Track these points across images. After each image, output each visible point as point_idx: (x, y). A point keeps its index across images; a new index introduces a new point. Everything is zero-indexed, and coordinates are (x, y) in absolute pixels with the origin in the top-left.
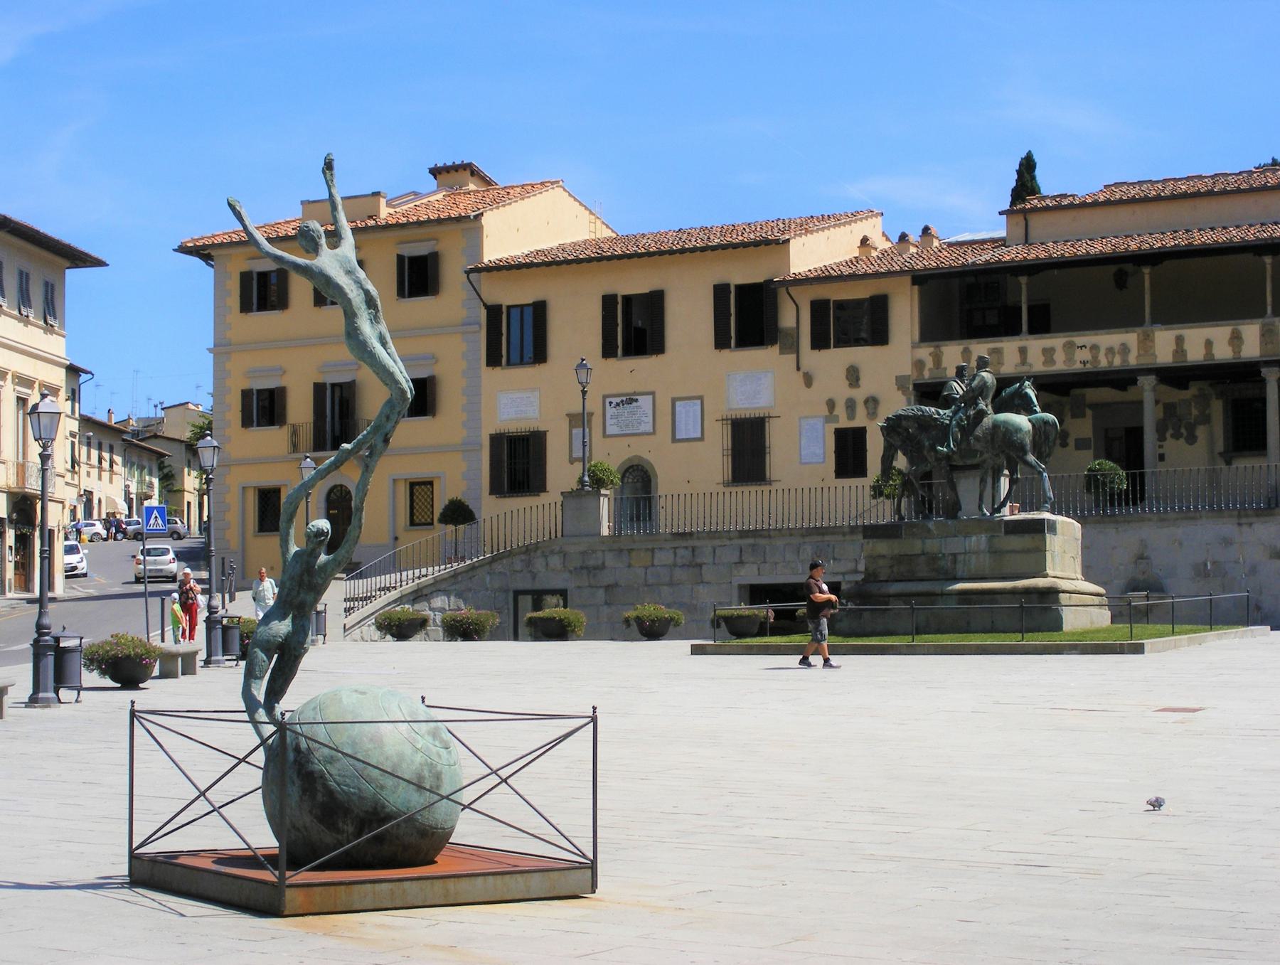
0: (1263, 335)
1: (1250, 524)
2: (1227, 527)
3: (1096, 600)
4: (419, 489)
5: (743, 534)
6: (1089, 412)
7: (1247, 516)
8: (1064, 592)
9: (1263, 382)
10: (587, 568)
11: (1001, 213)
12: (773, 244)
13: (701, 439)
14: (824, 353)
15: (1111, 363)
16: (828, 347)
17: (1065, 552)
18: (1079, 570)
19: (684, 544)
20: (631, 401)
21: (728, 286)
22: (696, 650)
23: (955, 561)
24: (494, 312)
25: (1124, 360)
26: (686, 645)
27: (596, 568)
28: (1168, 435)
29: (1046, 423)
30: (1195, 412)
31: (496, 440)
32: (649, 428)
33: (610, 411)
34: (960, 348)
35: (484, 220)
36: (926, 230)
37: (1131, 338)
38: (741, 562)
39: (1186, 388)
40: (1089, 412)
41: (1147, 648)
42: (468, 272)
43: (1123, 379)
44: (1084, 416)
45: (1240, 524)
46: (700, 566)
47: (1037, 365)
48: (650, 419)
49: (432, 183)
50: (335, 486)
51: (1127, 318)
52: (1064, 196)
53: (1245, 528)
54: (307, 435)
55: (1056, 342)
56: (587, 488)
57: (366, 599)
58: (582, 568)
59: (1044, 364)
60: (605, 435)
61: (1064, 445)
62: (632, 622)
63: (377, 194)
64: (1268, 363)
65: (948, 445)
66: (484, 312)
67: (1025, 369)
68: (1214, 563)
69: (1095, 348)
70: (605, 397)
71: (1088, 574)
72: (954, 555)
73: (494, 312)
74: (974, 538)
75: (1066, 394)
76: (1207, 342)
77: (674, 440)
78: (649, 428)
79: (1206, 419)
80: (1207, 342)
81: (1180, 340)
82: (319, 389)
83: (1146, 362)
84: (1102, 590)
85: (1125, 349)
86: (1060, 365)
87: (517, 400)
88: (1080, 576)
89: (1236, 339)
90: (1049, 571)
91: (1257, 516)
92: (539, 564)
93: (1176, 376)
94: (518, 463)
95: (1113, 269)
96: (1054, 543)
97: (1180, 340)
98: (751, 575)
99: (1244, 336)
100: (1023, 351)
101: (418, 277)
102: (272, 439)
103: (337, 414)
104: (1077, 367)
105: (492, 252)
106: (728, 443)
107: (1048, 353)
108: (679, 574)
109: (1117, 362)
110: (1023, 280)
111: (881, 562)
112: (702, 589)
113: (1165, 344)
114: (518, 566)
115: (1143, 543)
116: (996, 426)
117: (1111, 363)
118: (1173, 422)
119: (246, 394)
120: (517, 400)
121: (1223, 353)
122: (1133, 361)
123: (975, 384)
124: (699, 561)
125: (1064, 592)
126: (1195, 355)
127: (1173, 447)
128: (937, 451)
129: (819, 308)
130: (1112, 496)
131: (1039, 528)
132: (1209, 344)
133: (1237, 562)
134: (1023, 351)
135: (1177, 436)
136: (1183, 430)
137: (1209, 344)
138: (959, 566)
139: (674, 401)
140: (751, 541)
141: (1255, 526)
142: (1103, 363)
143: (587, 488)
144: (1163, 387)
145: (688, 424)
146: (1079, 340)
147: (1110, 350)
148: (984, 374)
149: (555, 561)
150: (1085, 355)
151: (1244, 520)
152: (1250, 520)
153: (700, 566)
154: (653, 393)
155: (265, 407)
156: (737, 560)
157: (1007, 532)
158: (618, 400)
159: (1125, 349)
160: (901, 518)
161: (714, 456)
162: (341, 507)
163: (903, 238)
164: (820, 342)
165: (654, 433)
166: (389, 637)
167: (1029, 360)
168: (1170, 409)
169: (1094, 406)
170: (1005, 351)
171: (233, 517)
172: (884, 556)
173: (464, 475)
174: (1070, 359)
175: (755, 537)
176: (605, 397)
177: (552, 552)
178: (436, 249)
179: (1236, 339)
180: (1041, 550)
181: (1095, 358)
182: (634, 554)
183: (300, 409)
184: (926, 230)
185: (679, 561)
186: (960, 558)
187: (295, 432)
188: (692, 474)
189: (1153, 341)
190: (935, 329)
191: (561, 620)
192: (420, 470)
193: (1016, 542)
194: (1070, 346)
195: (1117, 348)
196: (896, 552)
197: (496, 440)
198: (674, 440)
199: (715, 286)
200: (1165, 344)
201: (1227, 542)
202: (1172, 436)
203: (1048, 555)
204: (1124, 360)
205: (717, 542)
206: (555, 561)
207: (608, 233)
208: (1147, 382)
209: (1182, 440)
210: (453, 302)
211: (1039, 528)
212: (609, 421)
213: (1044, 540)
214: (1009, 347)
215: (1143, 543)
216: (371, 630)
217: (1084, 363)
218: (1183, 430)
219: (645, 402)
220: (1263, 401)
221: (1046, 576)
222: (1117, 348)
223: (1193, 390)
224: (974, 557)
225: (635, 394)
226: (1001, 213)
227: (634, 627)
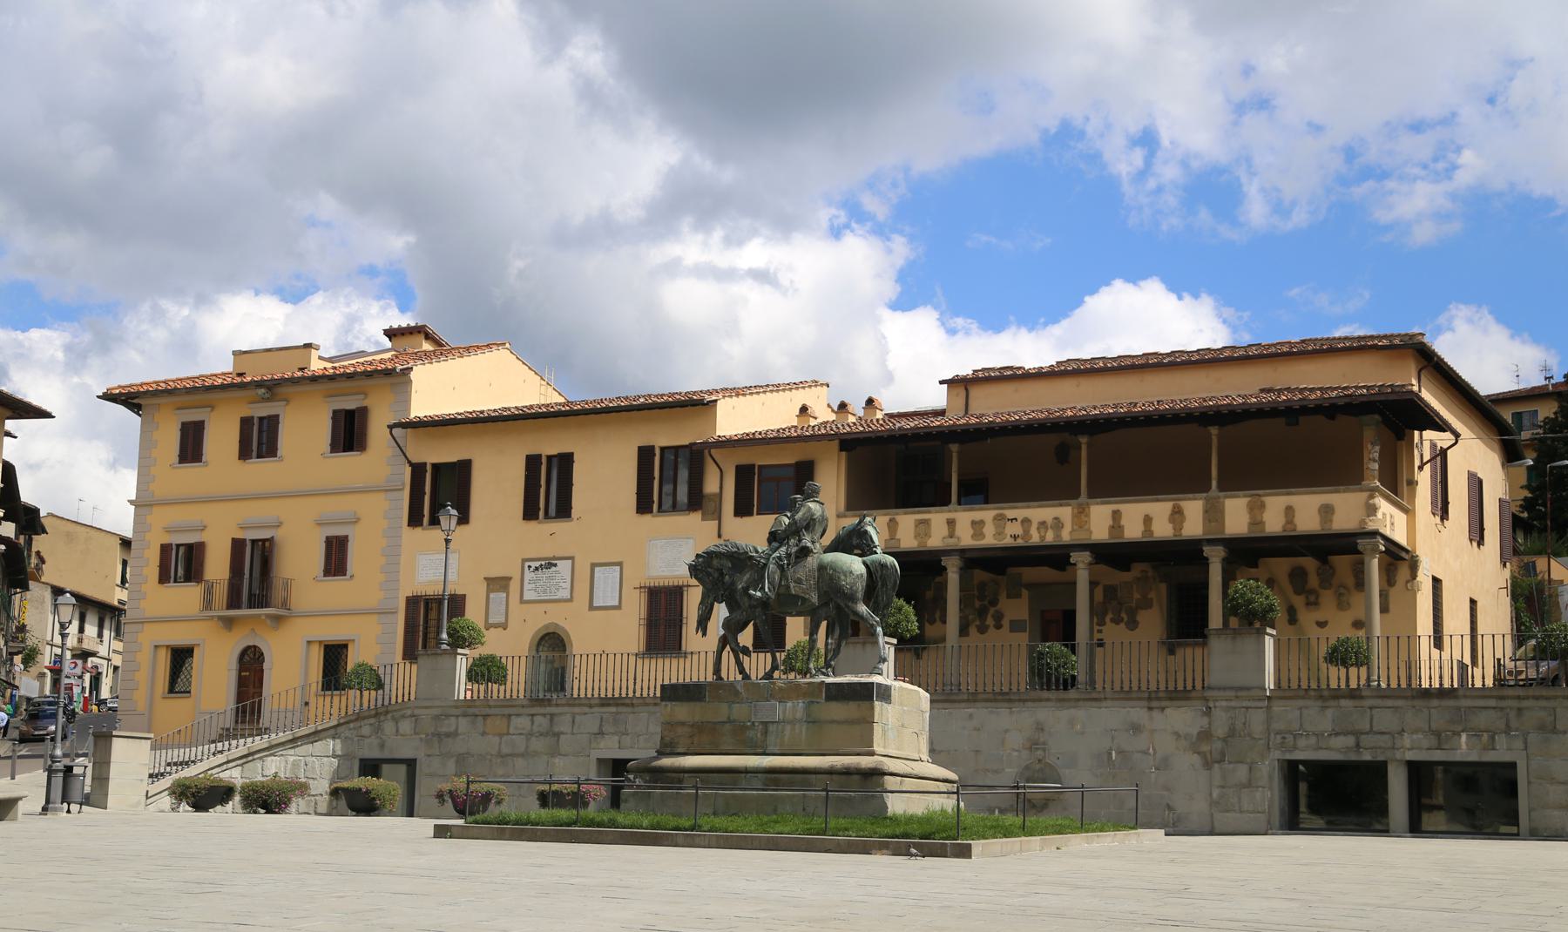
0: (1206, 511)
1: (1163, 709)
2: (1138, 713)
3: (943, 787)
4: (334, 654)
5: (605, 702)
6: (1025, 593)
7: (1158, 699)
8: (892, 774)
9: (1204, 563)
10: (439, 735)
11: (941, 382)
12: (698, 405)
13: (619, 607)
14: (747, 520)
15: (1043, 538)
16: (751, 514)
17: (903, 727)
18: (924, 747)
19: (542, 710)
20: (550, 565)
21: (653, 447)
22: (441, 832)
23: (765, 733)
24: (418, 470)
25: (1058, 536)
26: (428, 825)
27: (448, 735)
28: (1108, 619)
29: (883, 566)
30: (1137, 596)
31: (412, 602)
32: (566, 594)
33: (528, 575)
34: (887, 518)
35: (413, 375)
36: (870, 401)
37: (1065, 512)
38: (601, 733)
39: (1128, 570)
40: (1025, 593)
41: (974, 851)
42: (391, 427)
43: (1057, 557)
44: (1019, 596)
45: (1150, 709)
46: (558, 735)
47: (966, 539)
48: (568, 585)
49: (387, 343)
50: (249, 647)
51: (1061, 490)
52: (1011, 368)
53: (1155, 713)
54: (221, 593)
55: (987, 514)
56: (444, 647)
57: (187, 763)
58: (433, 735)
59: (974, 536)
60: (522, 601)
61: (998, 626)
62: (447, 798)
63: (308, 346)
64: (1211, 542)
65: (763, 588)
66: (408, 470)
67: (952, 541)
68: (1118, 753)
69: (1026, 522)
70: (524, 561)
71: (936, 754)
72: (765, 724)
73: (418, 470)
74: (789, 704)
75: (1003, 573)
76: (1145, 518)
77: (592, 608)
78: (566, 594)
79: (1148, 605)
80: (1145, 518)
81: (1116, 515)
82: (238, 545)
83: (1081, 537)
84: (953, 776)
85: (1058, 524)
86: (989, 539)
87: (428, 562)
88: (925, 757)
89: (1177, 515)
90: (877, 748)
91: (1171, 699)
92: (389, 727)
93: (1114, 555)
94: (431, 622)
95: (1053, 439)
96: (883, 712)
97: (1116, 515)
98: (611, 749)
99: (1186, 512)
100: (951, 523)
101: (349, 433)
102: (187, 596)
103: (255, 576)
104: (1008, 541)
105: (420, 407)
106: (644, 614)
107: (977, 525)
108: (537, 744)
109: (1050, 538)
110: (954, 448)
111: (680, 730)
112: (558, 761)
113: (1100, 521)
114: (366, 730)
115: (1040, 728)
116: (822, 568)
117: (1043, 538)
118: (1110, 605)
119: (165, 549)
120: (428, 562)
121: (1163, 530)
122: (1066, 537)
123: (799, 516)
124: (556, 729)
125: (892, 774)
126: (1133, 531)
127: (1113, 632)
128: (750, 596)
129: (744, 475)
130: (1057, 680)
131: (865, 694)
132: (1148, 520)
133: (1146, 753)
134: (951, 523)
135: (1117, 621)
136: (1124, 615)
137: (1148, 520)
138: (771, 739)
139: (593, 566)
140: (613, 709)
141: (1168, 711)
142: (1035, 538)
143: (444, 647)
144: (1102, 567)
145: (606, 592)
146: (1010, 513)
147: (1043, 524)
148: (811, 505)
149: (406, 726)
150: (1015, 529)
151: (1155, 704)
152: (1164, 704)
153: (558, 735)
154: (572, 558)
155: (183, 562)
156: (596, 730)
157: (829, 698)
158: (537, 564)
159: (1058, 524)
160: (720, 678)
161: (629, 629)
162: (251, 666)
163: (843, 406)
164: (742, 510)
165: (571, 600)
166: (184, 806)
167: (958, 532)
168: (1110, 592)
169: (1029, 586)
170: (933, 524)
171: (142, 676)
172: (683, 724)
173: (376, 643)
174: (999, 533)
175: (617, 705)
176: (524, 561)
177: (403, 717)
178: (365, 403)
179: (1177, 515)
180: (868, 722)
181: (1027, 532)
182: (489, 721)
183: (217, 566)
184: (870, 401)
185: (535, 728)
186: (771, 728)
187: (209, 591)
188: (608, 643)
189: (1088, 515)
190: (863, 496)
191: (368, 792)
192: (334, 631)
193: (838, 710)
194: (1000, 519)
195: (1049, 521)
196: (697, 718)
197: (412, 602)
198: (592, 608)
199: (640, 448)
200: (1100, 521)
201: (1136, 729)
202: (1112, 620)
203: (877, 729)
204: (1058, 536)
205: (576, 710)
206: (406, 726)
207: (562, 400)
208: (1081, 559)
209: (1122, 625)
210: (380, 460)
211: (865, 694)
212: (527, 586)
213: (872, 708)
214: (937, 518)
215: (1040, 728)
216: (166, 801)
217: (1015, 537)
218: (1124, 615)
219: (564, 567)
220: (1205, 585)
221: (872, 754)
222: (1049, 521)
223: (1138, 569)
224: (788, 727)
225: (555, 558)
226: (941, 382)
227: (449, 804)
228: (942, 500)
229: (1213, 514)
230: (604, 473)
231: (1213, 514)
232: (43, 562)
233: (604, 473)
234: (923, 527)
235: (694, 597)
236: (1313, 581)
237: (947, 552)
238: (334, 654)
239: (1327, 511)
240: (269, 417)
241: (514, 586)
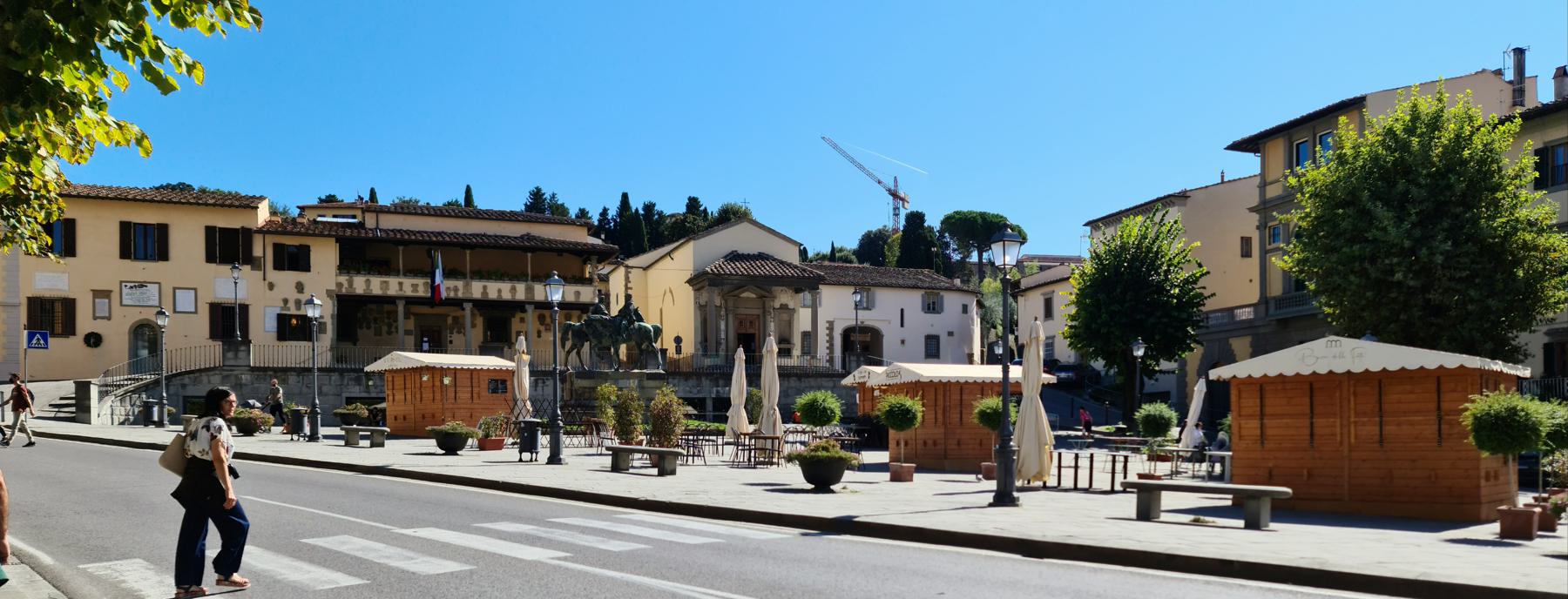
11: (468, 191)
33: (125, 291)
37: (460, 284)
47: (408, 292)
81: (485, 288)
83: (468, 296)
85: (456, 289)
89: (513, 289)
97: (485, 288)
109: (452, 295)
121: (507, 296)
122: (460, 295)
139: (196, 312)
179: (513, 289)
200: (477, 289)
208: (468, 307)
219: (153, 289)
226: (468, 191)
228: (397, 273)
229: (530, 290)
230: (187, 235)
231: (530, 290)
232: (331, 199)
233: (187, 235)
234: (385, 285)
235: (23, 168)
236: (548, 320)
237: (400, 298)
238: (144, 136)
239: (578, 294)
240: (159, 225)
241: (115, 297)
